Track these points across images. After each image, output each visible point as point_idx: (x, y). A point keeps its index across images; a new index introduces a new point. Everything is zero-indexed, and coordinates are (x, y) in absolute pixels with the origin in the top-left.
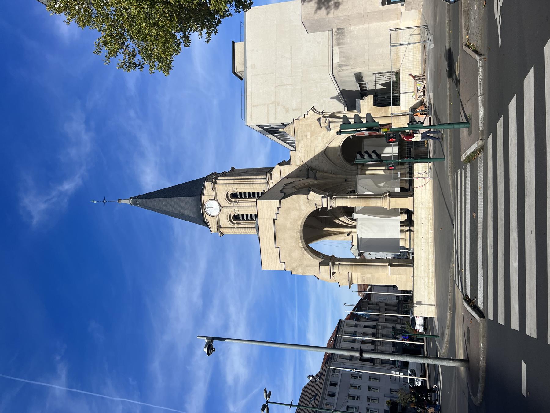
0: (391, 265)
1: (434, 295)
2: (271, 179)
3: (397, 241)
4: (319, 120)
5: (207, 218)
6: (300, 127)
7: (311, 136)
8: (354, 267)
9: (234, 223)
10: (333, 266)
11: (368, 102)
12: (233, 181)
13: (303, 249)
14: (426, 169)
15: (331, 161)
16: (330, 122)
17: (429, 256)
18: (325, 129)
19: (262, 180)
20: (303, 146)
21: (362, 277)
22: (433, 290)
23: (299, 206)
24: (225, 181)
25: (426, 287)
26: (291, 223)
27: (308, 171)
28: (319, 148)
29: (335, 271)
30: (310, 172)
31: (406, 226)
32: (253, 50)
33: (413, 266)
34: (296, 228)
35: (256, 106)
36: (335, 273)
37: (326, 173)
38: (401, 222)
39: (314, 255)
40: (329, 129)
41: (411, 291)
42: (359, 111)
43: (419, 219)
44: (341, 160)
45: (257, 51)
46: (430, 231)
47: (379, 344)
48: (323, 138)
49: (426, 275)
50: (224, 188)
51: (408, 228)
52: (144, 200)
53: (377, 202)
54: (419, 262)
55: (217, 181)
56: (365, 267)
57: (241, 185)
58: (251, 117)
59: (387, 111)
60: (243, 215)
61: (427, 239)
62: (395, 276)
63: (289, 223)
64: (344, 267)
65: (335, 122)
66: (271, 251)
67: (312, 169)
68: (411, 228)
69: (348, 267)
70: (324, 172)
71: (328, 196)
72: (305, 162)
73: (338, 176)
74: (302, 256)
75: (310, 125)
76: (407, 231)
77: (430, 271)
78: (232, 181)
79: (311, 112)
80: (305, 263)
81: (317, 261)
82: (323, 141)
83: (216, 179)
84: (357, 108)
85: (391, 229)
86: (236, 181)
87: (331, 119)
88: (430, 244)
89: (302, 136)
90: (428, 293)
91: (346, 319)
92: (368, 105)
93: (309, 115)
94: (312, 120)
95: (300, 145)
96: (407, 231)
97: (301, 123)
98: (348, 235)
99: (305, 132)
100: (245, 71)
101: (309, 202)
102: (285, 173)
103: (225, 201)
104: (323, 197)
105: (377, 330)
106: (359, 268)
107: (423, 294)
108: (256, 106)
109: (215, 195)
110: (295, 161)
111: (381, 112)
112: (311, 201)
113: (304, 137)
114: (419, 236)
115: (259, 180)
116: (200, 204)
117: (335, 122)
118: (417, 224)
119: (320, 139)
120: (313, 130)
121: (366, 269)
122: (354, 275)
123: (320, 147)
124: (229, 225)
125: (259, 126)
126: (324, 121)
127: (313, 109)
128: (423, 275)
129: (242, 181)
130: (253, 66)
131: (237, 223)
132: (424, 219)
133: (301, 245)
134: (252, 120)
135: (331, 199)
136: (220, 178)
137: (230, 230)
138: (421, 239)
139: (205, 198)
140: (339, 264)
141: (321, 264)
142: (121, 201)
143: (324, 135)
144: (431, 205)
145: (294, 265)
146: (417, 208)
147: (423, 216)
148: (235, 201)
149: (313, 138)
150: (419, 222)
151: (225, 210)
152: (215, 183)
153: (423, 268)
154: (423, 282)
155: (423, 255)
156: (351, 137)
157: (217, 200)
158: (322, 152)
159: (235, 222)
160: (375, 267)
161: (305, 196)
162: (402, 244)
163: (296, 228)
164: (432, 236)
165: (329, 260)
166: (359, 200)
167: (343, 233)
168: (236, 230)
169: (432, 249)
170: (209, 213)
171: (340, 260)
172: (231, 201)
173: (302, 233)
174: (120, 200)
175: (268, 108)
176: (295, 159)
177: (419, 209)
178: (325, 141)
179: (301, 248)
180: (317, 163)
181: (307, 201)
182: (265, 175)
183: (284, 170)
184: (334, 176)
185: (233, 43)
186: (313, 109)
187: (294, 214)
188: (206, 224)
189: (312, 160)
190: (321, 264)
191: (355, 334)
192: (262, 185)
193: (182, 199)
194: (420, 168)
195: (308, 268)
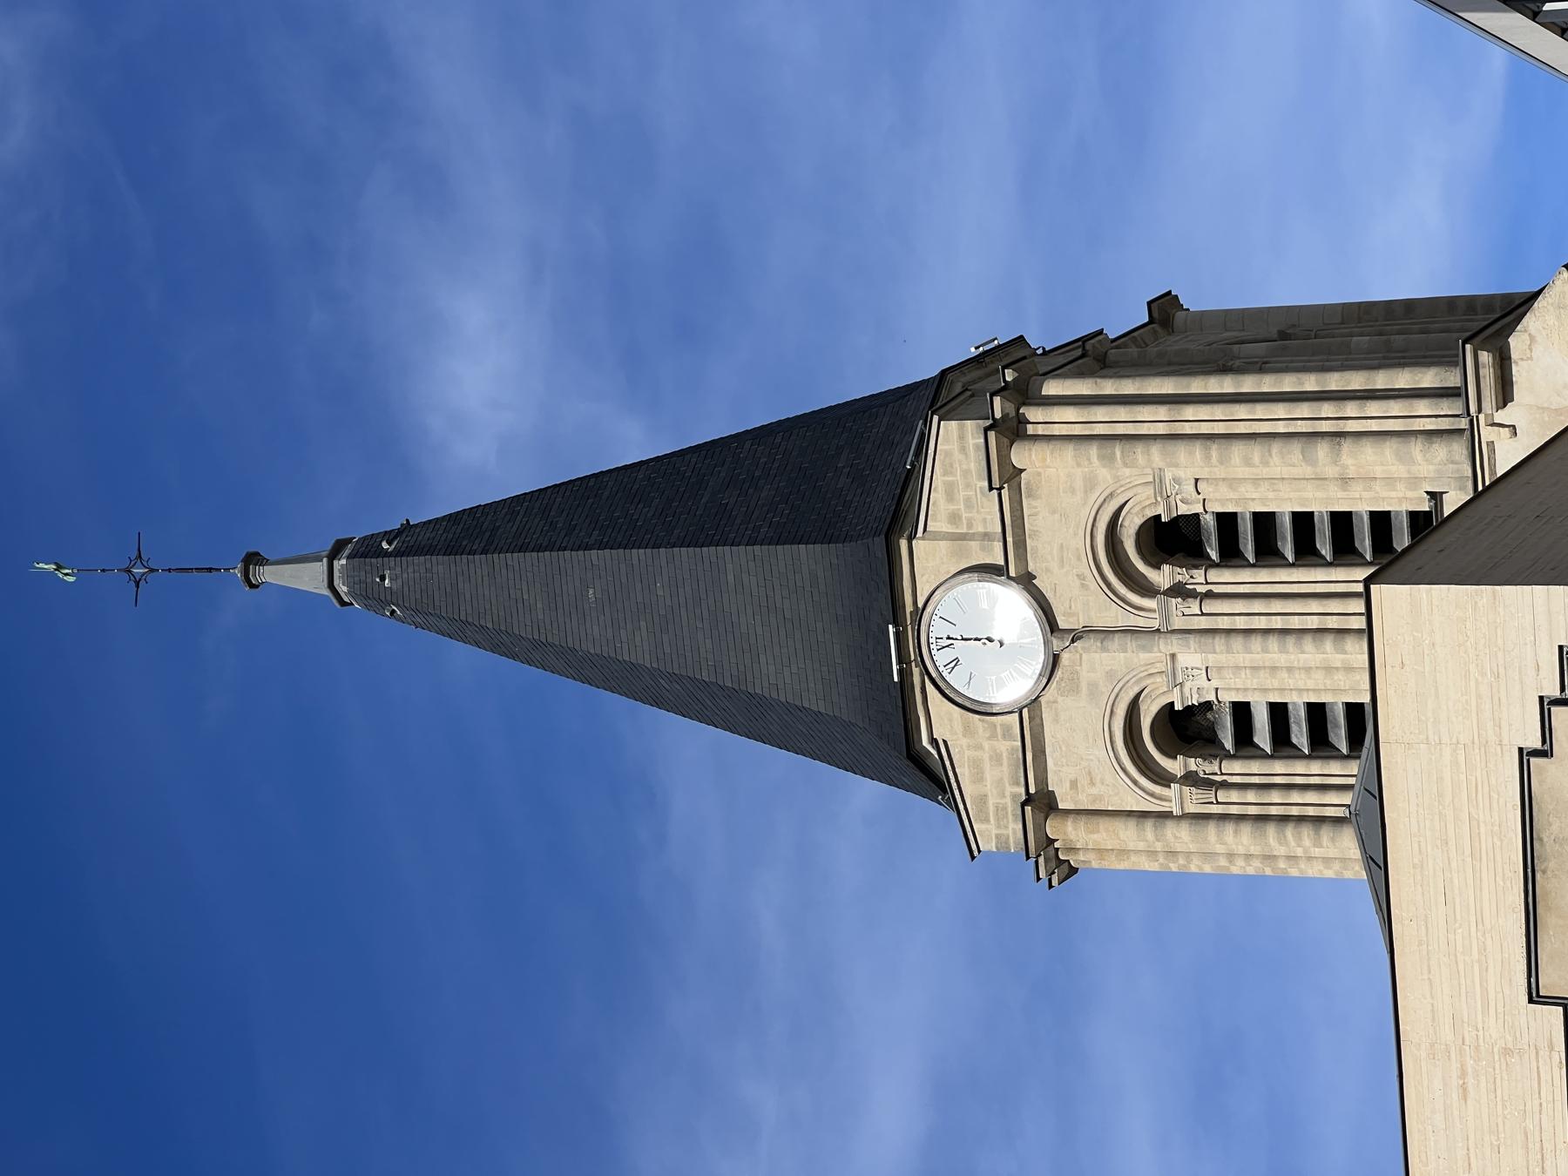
2: (1505, 394)
5: (941, 723)
9: (1164, 779)
12: (1162, 412)
19: (1422, 407)
24: (1100, 413)
50: (1086, 475)
52: (440, 566)
55: (1033, 414)
57: (1238, 450)
60: (1242, 712)
83: (1025, 393)
86: (1189, 412)
103: (1093, 581)
109: (1014, 530)
115: (1395, 407)
124: (1129, 792)
129: (1241, 411)
131: (1191, 779)
136: (1052, 388)
137: (1127, 834)
139: (927, 560)
148: (1179, 591)
151: (1085, 661)
152: (1013, 430)
157: (1026, 581)
159: (1175, 766)
168: (1180, 836)
182: (1451, 359)
188: (929, 776)
192: (1416, 448)
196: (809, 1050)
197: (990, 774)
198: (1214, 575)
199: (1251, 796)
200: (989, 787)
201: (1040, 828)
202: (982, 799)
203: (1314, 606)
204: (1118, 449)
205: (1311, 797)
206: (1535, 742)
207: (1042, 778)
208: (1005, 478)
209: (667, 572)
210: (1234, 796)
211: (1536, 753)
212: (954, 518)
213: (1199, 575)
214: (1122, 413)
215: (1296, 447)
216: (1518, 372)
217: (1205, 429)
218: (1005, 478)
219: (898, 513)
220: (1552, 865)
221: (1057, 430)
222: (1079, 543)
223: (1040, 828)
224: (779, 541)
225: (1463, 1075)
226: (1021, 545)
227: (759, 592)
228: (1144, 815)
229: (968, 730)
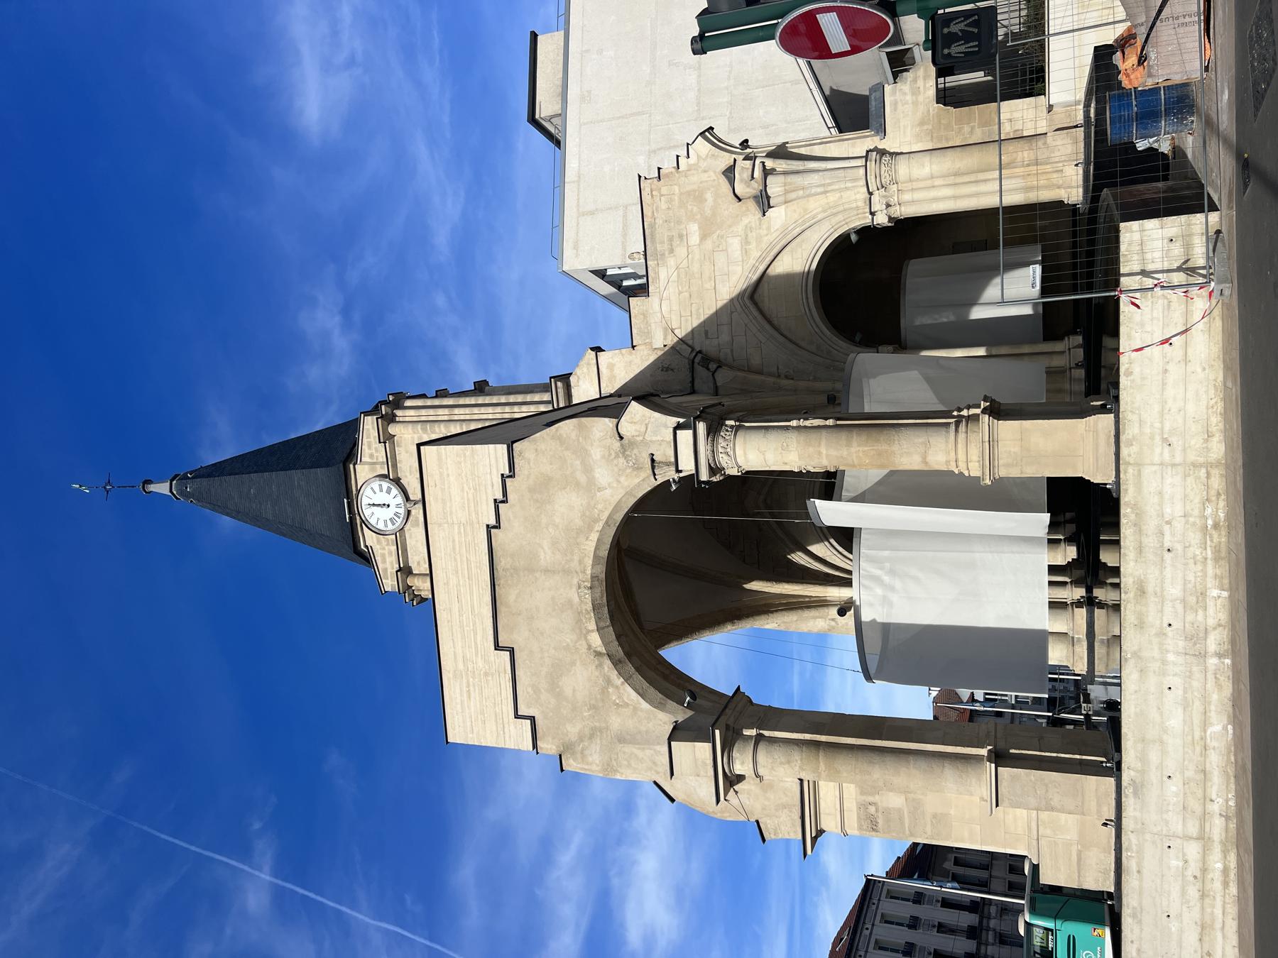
0: (1000, 758)
1: (1234, 939)
3: (1039, 640)
4: (729, 172)
5: (369, 539)
6: (664, 206)
7: (704, 237)
8: (822, 761)
10: (728, 746)
11: (916, 92)
12: (446, 411)
13: (607, 663)
14: (1188, 247)
15: (769, 322)
16: (766, 173)
17: (1205, 725)
18: (752, 206)
20: (674, 277)
21: (863, 806)
22: (1233, 910)
23: (588, 470)
24: (423, 412)
25: (1193, 892)
26: (554, 544)
27: (692, 370)
28: (731, 280)
29: (739, 769)
30: (700, 370)
31: (1076, 583)
32: (588, 51)
33: (1116, 770)
34: (575, 565)
35: (592, 213)
36: (740, 778)
37: (760, 373)
38: (1053, 569)
39: (652, 691)
40: (764, 202)
41: (1097, 897)
42: (882, 130)
43: (1151, 524)
44: (807, 319)
45: (600, 52)
46: (1215, 592)
47: (991, 939)
48: (746, 241)
49: (1193, 829)
51: (1079, 593)
52: (205, 481)
53: (927, 445)
54: (1154, 757)
55: (399, 413)
56: (876, 757)
58: (576, 247)
61: (1195, 637)
62: (1022, 813)
63: (546, 544)
64: (779, 753)
65: (785, 173)
66: (480, 663)
67: (706, 360)
68: (1099, 593)
69: (797, 756)
70: (749, 370)
71: (697, 418)
72: (681, 333)
73: (802, 384)
74: (604, 691)
76: (1078, 604)
77: (1215, 808)
79: (702, 146)
80: (616, 722)
81: (663, 720)
82: (746, 252)
84: (872, 122)
85: (1001, 580)
86: (456, 411)
87: (770, 163)
88: (1213, 661)
89: (671, 239)
90: (1204, 928)
91: (889, 874)
92: (915, 103)
94: (704, 177)
95: (663, 273)
96: (1078, 604)
98: (842, 612)
99: (679, 222)
100: (562, 115)
101: (624, 449)
102: (612, 378)
104: (679, 427)
105: (981, 918)
106: (845, 765)
107: (1174, 926)
108: (592, 213)
109: (392, 460)
110: (648, 334)
111: (966, 129)
112: (632, 444)
113: (676, 242)
114: (1152, 617)
116: (346, 491)
117: (785, 173)
118: (1140, 549)
119: (735, 244)
120: (708, 212)
121: (879, 772)
122: (828, 792)
123: (734, 279)
125: (601, 274)
126: (747, 174)
127: (708, 133)
128: (1177, 827)
129: (476, 410)
130: (585, 98)
132: (1179, 525)
133: (596, 640)
134: (577, 255)
135: (713, 431)
136: (408, 403)
138: (1161, 634)
139: (362, 472)
140: (759, 738)
141: (678, 733)
143: (748, 228)
144: (1218, 449)
145: (573, 730)
146: (1139, 465)
147: (1174, 509)
149: (709, 244)
150: (1150, 541)
152: (391, 419)
153: (1173, 787)
154: (1175, 863)
155: (1175, 721)
156: (854, 238)
157: (397, 482)
158: (741, 295)
160: (923, 763)
162: (1056, 655)
163: (575, 565)
164: (1223, 616)
165: (721, 719)
166: (843, 435)
167: (822, 603)
169: (1228, 689)
170: (373, 521)
171: (771, 717)
173: (600, 591)
175: (625, 216)
177: (1147, 471)
178: (756, 254)
179: (598, 654)
180: (725, 337)
181: (617, 444)
183: (611, 367)
184: (785, 382)
185: (534, 36)
186: (708, 133)
188: (366, 558)
189: (705, 329)
190: (678, 733)
191: (914, 923)
193: (296, 475)
194: (1147, 243)
195: (629, 749)
197: (388, 560)
200: (388, 565)
201: (404, 581)
202: (385, 570)
204: (428, 426)
206: (493, 522)
207: (406, 561)
208: (387, 439)
209: (274, 480)
211: (495, 527)
212: (371, 456)
214: (431, 412)
217: (462, 417)
218: (387, 439)
219: (350, 454)
220: (502, 582)
221: (407, 419)
223: (404, 581)
224: (311, 467)
225: (468, 686)
226: (395, 466)
227: (304, 484)
229: (379, 542)
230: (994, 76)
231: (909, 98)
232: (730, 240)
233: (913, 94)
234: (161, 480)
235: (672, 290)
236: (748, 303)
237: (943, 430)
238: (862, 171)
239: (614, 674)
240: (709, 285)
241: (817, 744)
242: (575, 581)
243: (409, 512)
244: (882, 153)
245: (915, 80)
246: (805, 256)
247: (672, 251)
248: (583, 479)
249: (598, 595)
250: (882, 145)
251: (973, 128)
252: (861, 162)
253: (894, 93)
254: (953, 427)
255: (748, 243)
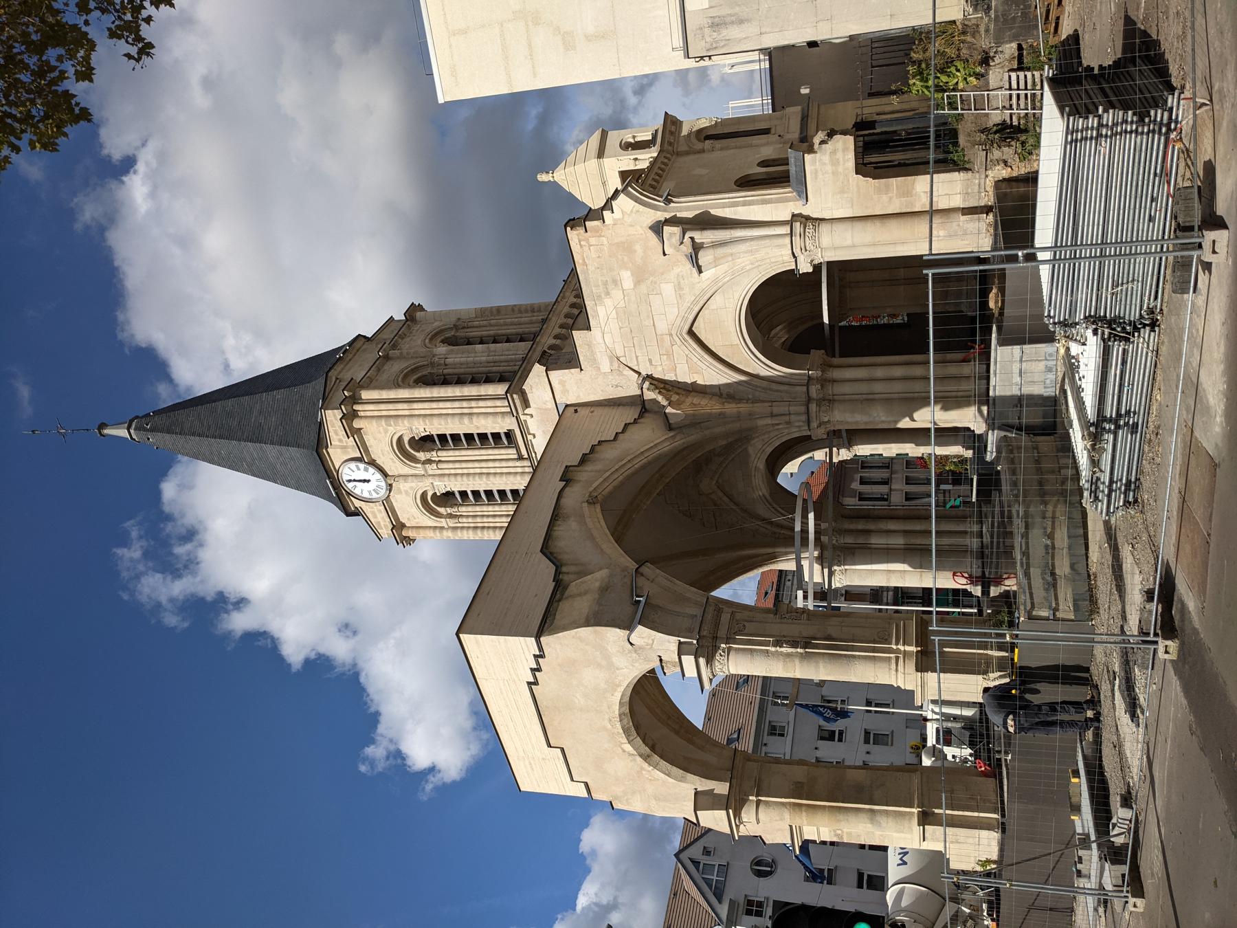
2: (526, 404)
4: (657, 228)
6: (594, 255)
7: (637, 283)
11: (835, 163)
12: (405, 406)
13: (639, 759)
35: (464, 32)
39: (675, 770)
42: (803, 194)
48: (678, 287)
59: (907, 193)
75: (626, 247)
78: (403, 409)
83: (355, 399)
86: (415, 406)
89: (605, 284)
92: (835, 173)
93: (618, 213)
95: (601, 311)
97: (593, 241)
108: (464, 32)
109: (363, 446)
111: (885, 198)
113: (610, 286)
119: (668, 289)
124: (429, 521)
126: (676, 240)
131: (451, 516)
133: (628, 748)
135: (710, 661)
136: (365, 395)
142: (106, 431)
149: (643, 288)
157: (372, 463)
159: (442, 510)
161: (622, 633)
172: (415, 460)
174: (102, 426)
176: (593, 353)
187: (591, 677)
196: (963, 2)
197: (379, 516)
198: (440, 453)
199: (470, 520)
201: (400, 535)
203: (477, 465)
205: (490, 520)
207: (397, 518)
210: (465, 520)
213: (434, 453)
215: (457, 419)
216: (530, 396)
217: (423, 412)
222: (388, 449)
226: (366, 450)
228: (435, 528)
230: (942, 653)
231: (829, 168)
232: (663, 286)
233: (833, 165)
234: (117, 424)
235: (614, 325)
236: (687, 338)
237: (885, 665)
238: (788, 240)
239: (646, 765)
240: (648, 322)
241: (800, 805)
242: (607, 717)
243: (391, 485)
244: (807, 219)
245: (834, 152)
246: (736, 297)
247: (608, 294)
248: (604, 663)
249: (625, 721)
250: (806, 211)
251: (891, 198)
252: (785, 230)
253: (814, 162)
254: (893, 661)
255: (681, 288)
